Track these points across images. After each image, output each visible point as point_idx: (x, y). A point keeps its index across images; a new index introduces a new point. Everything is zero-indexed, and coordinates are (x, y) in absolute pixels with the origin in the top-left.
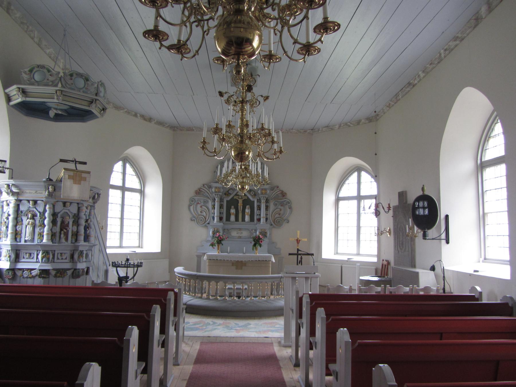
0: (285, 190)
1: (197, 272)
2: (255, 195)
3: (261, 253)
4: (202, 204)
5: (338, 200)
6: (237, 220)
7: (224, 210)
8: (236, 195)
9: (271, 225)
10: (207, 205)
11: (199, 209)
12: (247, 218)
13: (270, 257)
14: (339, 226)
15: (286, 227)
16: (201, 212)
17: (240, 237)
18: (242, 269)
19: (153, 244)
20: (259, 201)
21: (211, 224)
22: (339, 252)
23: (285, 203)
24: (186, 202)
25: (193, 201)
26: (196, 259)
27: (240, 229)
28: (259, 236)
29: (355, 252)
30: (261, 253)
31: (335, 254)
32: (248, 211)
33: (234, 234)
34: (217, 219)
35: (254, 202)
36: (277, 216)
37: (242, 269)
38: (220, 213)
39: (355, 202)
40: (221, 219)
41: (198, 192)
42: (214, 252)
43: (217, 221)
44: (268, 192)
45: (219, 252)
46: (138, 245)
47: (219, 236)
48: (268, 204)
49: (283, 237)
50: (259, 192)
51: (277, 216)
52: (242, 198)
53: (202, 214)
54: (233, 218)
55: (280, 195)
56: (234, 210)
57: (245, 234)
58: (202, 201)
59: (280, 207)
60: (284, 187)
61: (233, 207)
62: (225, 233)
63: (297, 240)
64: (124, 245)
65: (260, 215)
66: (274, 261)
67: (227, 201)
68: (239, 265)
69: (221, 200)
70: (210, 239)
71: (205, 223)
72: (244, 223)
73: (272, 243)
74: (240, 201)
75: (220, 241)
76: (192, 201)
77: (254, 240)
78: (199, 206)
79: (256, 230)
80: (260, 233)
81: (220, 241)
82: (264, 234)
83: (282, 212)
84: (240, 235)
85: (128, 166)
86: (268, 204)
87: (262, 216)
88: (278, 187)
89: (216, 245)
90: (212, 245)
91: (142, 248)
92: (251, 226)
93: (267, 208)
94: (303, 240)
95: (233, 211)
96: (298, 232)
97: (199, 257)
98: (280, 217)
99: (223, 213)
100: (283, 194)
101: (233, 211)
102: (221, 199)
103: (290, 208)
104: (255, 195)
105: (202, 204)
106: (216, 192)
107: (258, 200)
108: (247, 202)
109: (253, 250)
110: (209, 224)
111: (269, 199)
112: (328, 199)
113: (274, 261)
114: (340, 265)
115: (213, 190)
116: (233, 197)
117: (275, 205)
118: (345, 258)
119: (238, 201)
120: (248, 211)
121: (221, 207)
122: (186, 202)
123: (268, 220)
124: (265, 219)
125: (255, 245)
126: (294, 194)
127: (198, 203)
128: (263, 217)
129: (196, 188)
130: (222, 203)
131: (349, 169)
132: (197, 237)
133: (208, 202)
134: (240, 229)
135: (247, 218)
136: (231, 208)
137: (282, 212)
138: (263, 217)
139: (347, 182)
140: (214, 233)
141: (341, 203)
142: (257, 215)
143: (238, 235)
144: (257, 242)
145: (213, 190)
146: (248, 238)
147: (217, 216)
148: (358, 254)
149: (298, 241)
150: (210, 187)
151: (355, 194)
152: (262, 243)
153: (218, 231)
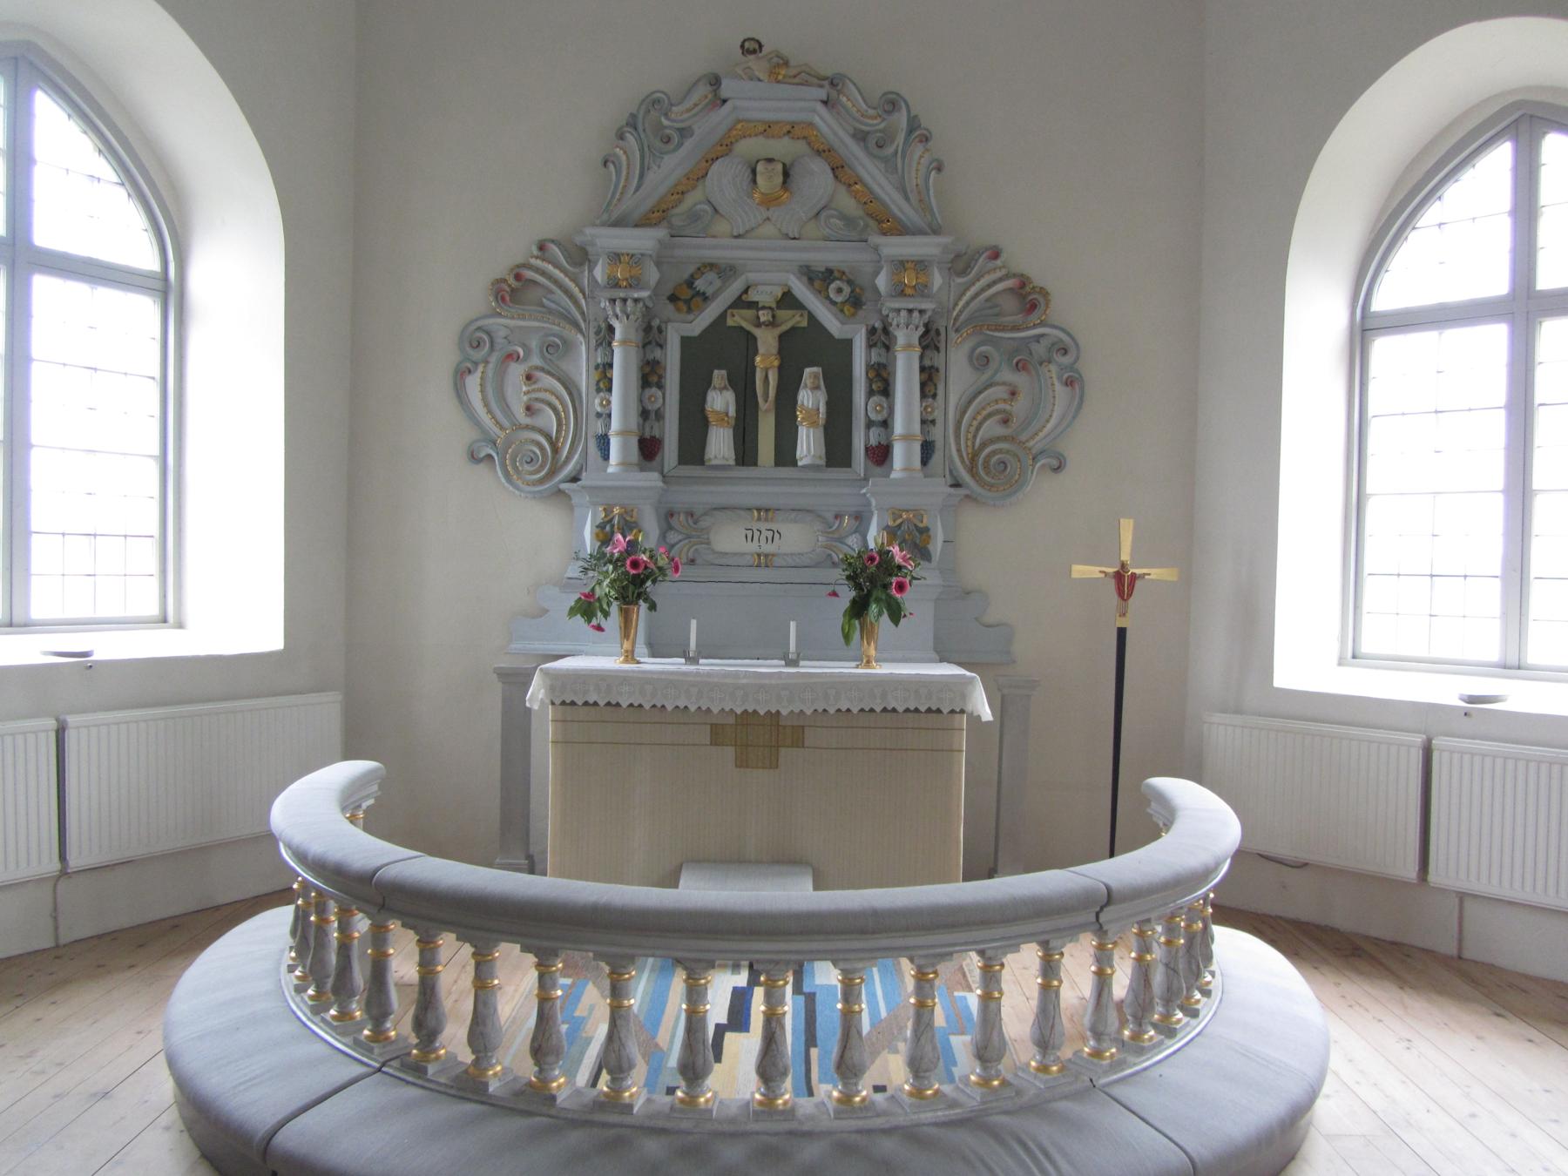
0: (1039, 276)
1: (626, 661)
2: (856, 302)
3: (900, 664)
4: (536, 361)
5: (1365, 329)
6: (746, 453)
7: (670, 398)
8: (740, 303)
9: (956, 485)
10: (565, 366)
11: (517, 393)
12: (808, 444)
13: (960, 686)
14: (1370, 487)
15: (1043, 497)
16: (528, 408)
17: (765, 561)
18: (773, 764)
19: (241, 606)
20: (881, 338)
21: (586, 479)
22: (1365, 648)
23: (1039, 349)
24: (439, 352)
25: (478, 345)
26: (494, 696)
27: (765, 512)
28: (884, 553)
29: (1492, 652)
30: (900, 664)
31: (1340, 664)
32: (810, 398)
33: (730, 538)
34: (624, 448)
35: (847, 344)
36: (991, 428)
37: (773, 764)
38: (644, 414)
39: (1495, 337)
40: (649, 449)
41: (513, 290)
42: (599, 658)
43: (624, 464)
44: (937, 280)
45: (630, 657)
46: (153, 610)
47: (632, 546)
48: (938, 360)
49: (1033, 556)
50: (882, 282)
51: (991, 428)
52: (772, 324)
53: (538, 421)
54: (720, 444)
55: (1010, 304)
56: (730, 396)
57: (796, 538)
58: (534, 344)
59: (1007, 375)
60: (1026, 257)
61: (719, 376)
62: (673, 537)
63: (1119, 576)
64: (36, 613)
65: (886, 424)
66: (986, 714)
67: (686, 342)
68: (759, 736)
69: (650, 336)
70: (574, 570)
71: (550, 472)
72: (785, 472)
73: (959, 594)
74: (767, 342)
75: (639, 581)
76: (475, 340)
77: (852, 578)
78: (516, 371)
79: (861, 519)
80: (892, 533)
81: (635, 584)
82: (917, 541)
83: (1019, 407)
84: (768, 548)
85: (47, 110)
86: (938, 360)
87: (899, 427)
88: (996, 254)
89: (614, 609)
90: (587, 608)
91: (180, 625)
92: (836, 491)
93: (929, 380)
94: (1155, 573)
95: (721, 401)
96: (1127, 529)
97: (517, 680)
98: (1010, 439)
99: (659, 416)
100: (1029, 298)
101: (721, 401)
102: (648, 329)
103: (1069, 383)
104: (856, 302)
105: (536, 361)
106: (614, 284)
107: (872, 331)
108: (806, 347)
109: (847, 637)
110: (575, 479)
111: (941, 324)
112: (1313, 313)
113: (986, 714)
114: (1419, 739)
115: (599, 273)
116: (723, 316)
117: (981, 362)
118: (1446, 691)
119: (751, 340)
120: (810, 398)
121: (650, 375)
122: (443, 354)
123: (937, 458)
124: (917, 448)
125: (858, 609)
126: (1095, 297)
127: (511, 357)
128: (907, 438)
129: (500, 265)
130: (658, 353)
131: (1466, 114)
132: (502, 560)
133: (568, 346)
134: (765, 512)
135: (808, 444)
136: (708, 384)
137: (1019, 407)
138: (907, 438)
139: (1433, 214)
140: (604, 535)
141: (1383, 348)
142: (870, 424)
143: (753, 547)
144: (873, 588)
145: (599, 273)
146: (817, 565)
147: (623, 433)
148: (1513, 666)
149: (1124, 583)
150: (581, 257)
151: (1497, 284)
152: (907, 599)
153: (628, 526)
